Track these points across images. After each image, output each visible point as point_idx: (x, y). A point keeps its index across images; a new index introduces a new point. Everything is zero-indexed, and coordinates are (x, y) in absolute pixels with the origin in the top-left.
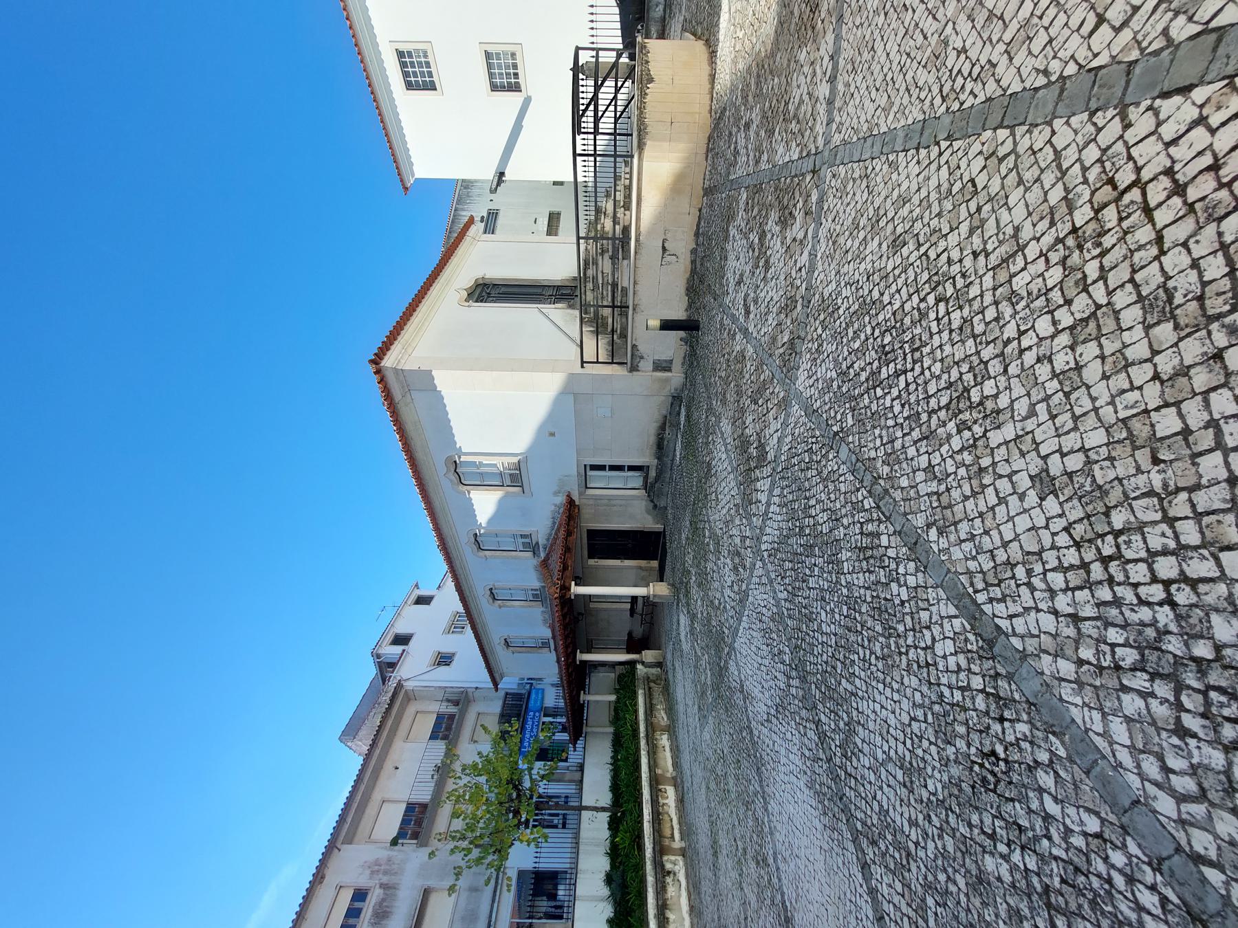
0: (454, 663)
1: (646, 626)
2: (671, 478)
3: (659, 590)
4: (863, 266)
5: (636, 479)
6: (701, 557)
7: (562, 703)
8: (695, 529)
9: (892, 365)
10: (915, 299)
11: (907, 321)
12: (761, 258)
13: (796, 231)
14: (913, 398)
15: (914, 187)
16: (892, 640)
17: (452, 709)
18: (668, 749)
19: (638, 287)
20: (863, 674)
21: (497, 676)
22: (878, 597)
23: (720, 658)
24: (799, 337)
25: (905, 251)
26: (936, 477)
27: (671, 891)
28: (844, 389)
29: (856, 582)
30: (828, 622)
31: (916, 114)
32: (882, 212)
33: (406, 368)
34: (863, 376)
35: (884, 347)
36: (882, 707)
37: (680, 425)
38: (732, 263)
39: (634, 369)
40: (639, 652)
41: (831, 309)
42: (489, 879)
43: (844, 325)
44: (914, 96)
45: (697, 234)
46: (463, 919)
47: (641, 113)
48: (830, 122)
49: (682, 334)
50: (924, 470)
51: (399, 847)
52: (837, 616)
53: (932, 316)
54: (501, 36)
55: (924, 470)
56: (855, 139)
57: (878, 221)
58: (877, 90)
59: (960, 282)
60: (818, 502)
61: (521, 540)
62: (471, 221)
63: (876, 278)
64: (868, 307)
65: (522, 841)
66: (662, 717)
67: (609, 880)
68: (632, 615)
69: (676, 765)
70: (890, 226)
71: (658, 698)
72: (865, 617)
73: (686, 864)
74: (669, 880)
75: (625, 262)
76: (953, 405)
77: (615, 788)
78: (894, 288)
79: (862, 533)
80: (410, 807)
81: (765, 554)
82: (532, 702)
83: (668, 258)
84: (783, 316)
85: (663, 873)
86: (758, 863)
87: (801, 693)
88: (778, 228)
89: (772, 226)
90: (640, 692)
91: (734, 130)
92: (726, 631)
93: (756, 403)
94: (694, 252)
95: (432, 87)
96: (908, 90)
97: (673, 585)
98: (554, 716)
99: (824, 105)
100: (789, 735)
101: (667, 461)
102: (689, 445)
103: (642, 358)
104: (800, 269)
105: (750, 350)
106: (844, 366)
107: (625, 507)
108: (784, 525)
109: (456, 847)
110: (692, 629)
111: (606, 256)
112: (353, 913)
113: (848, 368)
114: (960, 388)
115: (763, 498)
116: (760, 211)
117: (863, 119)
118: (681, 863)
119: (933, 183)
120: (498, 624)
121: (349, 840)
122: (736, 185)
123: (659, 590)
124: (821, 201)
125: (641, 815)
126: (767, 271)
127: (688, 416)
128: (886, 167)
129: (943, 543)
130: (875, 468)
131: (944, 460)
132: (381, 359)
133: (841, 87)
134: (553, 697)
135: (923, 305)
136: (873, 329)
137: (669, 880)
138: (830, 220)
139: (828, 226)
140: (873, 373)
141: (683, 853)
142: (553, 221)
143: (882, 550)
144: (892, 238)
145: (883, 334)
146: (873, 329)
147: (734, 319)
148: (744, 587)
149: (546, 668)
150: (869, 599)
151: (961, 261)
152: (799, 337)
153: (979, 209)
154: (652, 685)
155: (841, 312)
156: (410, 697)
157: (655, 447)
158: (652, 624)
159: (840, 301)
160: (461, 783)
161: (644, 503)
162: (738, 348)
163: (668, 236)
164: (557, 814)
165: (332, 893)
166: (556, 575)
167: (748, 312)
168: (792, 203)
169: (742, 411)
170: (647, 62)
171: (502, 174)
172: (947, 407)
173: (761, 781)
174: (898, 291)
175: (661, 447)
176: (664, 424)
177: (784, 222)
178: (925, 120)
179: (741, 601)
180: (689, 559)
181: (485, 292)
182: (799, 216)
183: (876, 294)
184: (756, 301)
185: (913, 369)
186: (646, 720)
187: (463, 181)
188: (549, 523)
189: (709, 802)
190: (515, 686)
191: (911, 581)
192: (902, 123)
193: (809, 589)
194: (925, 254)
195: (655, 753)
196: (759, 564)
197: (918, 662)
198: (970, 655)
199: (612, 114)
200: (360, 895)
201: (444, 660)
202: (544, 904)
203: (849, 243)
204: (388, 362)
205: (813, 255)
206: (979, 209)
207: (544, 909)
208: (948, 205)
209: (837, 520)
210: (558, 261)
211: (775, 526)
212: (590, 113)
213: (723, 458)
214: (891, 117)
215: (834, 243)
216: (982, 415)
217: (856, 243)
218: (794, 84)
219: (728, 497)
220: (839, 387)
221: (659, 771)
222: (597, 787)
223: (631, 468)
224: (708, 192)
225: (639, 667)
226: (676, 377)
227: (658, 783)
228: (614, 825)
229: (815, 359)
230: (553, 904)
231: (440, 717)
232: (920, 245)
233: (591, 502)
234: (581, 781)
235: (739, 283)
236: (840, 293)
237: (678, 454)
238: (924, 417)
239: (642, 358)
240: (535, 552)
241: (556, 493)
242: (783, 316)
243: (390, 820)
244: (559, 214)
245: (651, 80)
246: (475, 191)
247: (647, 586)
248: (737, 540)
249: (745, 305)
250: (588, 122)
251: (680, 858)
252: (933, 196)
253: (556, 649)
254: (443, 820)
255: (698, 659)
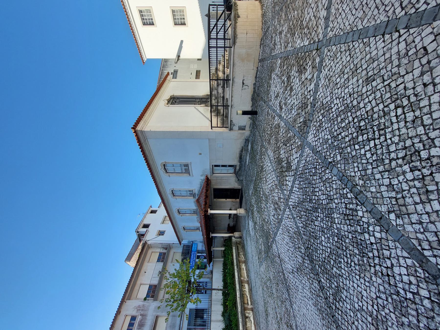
0: (165, 234)
1: (235, 225)
2: (245, 169)
3: (241, 211)
4: (347, 90)
5: (231, 170)
6: (259, 201)
7: (204, 249)
8: (255, 189)
9: (365, 136)
10: (381, 106)
11: (376, 116)
12: (288, 86)
13: (308, 74)
14: (379, 152)
15: (381, 53)
16: (365, 259)
17: (165, 251)
18: (245, 269)
19: (233, 98)
20: (346, 269)
21: (181, 240)
22: (356, 237)
23: (268, 242)
24: (309, 120)
25: (374, 84)
26: (394, 190)
27: (248, 324)
28: (335, 144)
29: (343, 228)
30: (325, 243)
31: (383, 18)
32: (359, 66)
33: (146, 130)
34: (347, 139)
35: (360, 127)
36: (358, 286)
37: (250, 150)
38: (273, 88)
39: (231, 129)
40: (233, 233)
41: (327, 109)
42: (180, 315)
43: (335, 116)
44: (382, 9)
45: (256, 77)
46: (170, 326)
47: (235, 30)
48: (327, 27)
49: (250, 116)
50: (387, 186)
51: (147, 301)
52: (331, 241)
53: (393, 114)
54: (178, 4)
55: (387, 186)
56: (342, 33)
57: (356, 70)
58: (356, 10)
59: (413, 99)
60: (320, 190)
61: (189, 192)
62: (168, 74)
63: (355, 96)
64: (348, 109)
65: (191, 302)
66: (242, 258)
67: (223, 315)
68: (229, 219)
69: (248, 276)
70: (364, 72)
71: (240, 250)
72: (348, 245)
73: (253, 314)
74: (247, 320)
75: (227, 89)
76: (408, 158)
77: (224, 280)
78: (367, 100)
79: (346, 208)
80: (150, 286)
81: (291, 207)
82: (193, 248)
83: (245, 87)
84: (300, 111)
85: (245, 318)
86: (287, 326)
87: (310, 267)
88: (297, 74)
89: (294, 73)
90: (234, 248)
91: (274, 35)
92: (271, 232)
93: (286, 145)
94: (255, 84)
95: (152, 24)
96: (377, 7)
97: (246, 209)
98: (201, 253)
99: (323, 20)
100: (304, 282)
101: (243, 163)
102: (253, 158)
103: (234, 125)
104: (310, 91)
105: (282, 124)
106: (335, 134)
107: (229, 181)
108: (301, 197)
109: (168, 305)
110: (255, 228)
111: (220, 87)
112: (131, 325)
113: (338, 135)
114: (413, 150)
115: (290, 184)
116: (287, 67)
117: (347, 24)
118: (251, 313)
119: (395, 50)
120: (181, 222)
121: (129, 299)
122: (275, 57)
123: (241, 211)
124: (321, 62)
125: (236, 295)
126: (291, 92)
127: (252, 147)
128: (361, 45)
129: (399, 221)
130: (354, 181)
131: (401, 183)
132: (136, 127)
133: (333, 11)
134: (201, 246)
135: (386, 109)
136: (354, 119)
137: (247, 320)
138: (326, 70)
139: (325, 73)
140: (353, 138)
141: (252, 310)
142: (198, 74)
143: (359, 218)
144: (366, 77)
145: (359, 122)
146: (354, 119)
147: (274, 111)
148: (280, 217)
149: (197, 238)
150: (350, 237)
151: (414, 88)
152: (309, 120)
153: (429, 62)
154: (238, 245)
155: (333, 110)
156: (149, 247)
157: (239, 158)
158: (237, 221)
159: (333, 105)
160: (169, 281)
161: (234, 178)
162: (276, 122)
163: (245, 78)
164: (203, 289)
165: (124, 317)
166: (203, 206)
167: (281, 108)
168: (305, 63)
169: (279, 148)
170: (237, 10)
171: (179, 56)
172: (403, 158)
173: (289, 295)
174: (370, 102)
175: (241, 157)
176: (242, 150)
177: (301, 71)
178: (388, 21)
179: (278, 222)
180: (253, 201)
181: (174, 100)
182: (309, 70)
183: (355, 103)
184: (285, 104)
185: (379, 138)
186: (236, 259)
187: (165, 59)
188: (199, 186)
189: (263, 294)
190: (187, 243)
191: (378, 235)
192: (373, 23)
193: (315, 226)
194: (389, 85)
195: (240, 271)
196: (287, 210)
197: (382, 273)
198: (419, 279)
199: (223, 30)
200: (133, 318)
201: (161, 233)
202: (199, 321)
203: (338, 80)
204: (139, 128)
205: (317, 85)
206: (429, 62)
207: (199, 323)
208: (405, 61)
209: (331, 200)
210: (202, 88)
211: (296, 196)
212: (215, 30)
213: (269, 165)
214: (366, 21)
215: (329, 80)
216: (429, 165)
217: (343, 80)
218: (306, 12)
219: (272, 181)
220: (332, 143)
221: (242, 279)
222: (217, 281)
223: (230, 166)
224: (261, 61)
225: (233, 238)
226: (247, 133)
227: (242, 283)
228: (224, 294)
229: (318, 130)
230: (202, 321)
231: (160, 254)
232: (384, 81)
233: (215, 178)
234: (212, 278)
235: (277, 97)
236: (333, 102)
237: (248, 161)
238: (387, 161)
239: (234, 125)
240: (194, 196)
241: (202, 176)
242: (300, 111)
243: (143, 291)
244: (200, 71)
245: (239, 17)
246: (169, 63)
247: (236, 210)
248: (277, 198)
249: (280, 105)
250: (213, 35)
251: (251, 312)
252: (394, 57)
253: (202, 231)
254: (162, 294)
255: (257, 239)
